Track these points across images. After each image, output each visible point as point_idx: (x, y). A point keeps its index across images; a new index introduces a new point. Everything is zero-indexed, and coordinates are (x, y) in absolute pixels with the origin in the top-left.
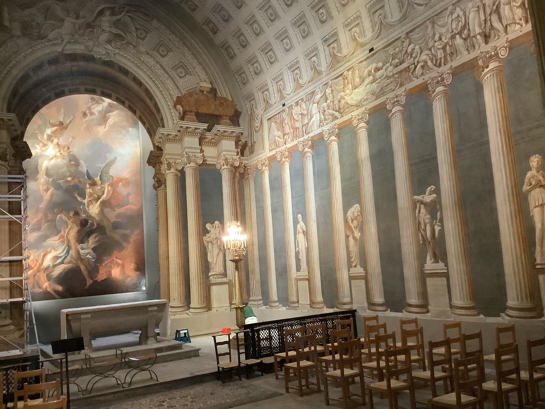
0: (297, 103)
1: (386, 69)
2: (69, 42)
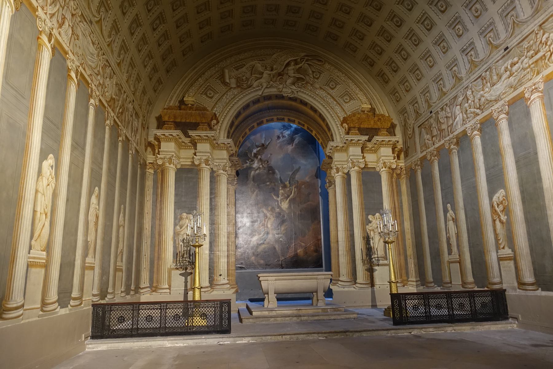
0: (442, 109)
1: (522, 62)
2: (266, 88)
